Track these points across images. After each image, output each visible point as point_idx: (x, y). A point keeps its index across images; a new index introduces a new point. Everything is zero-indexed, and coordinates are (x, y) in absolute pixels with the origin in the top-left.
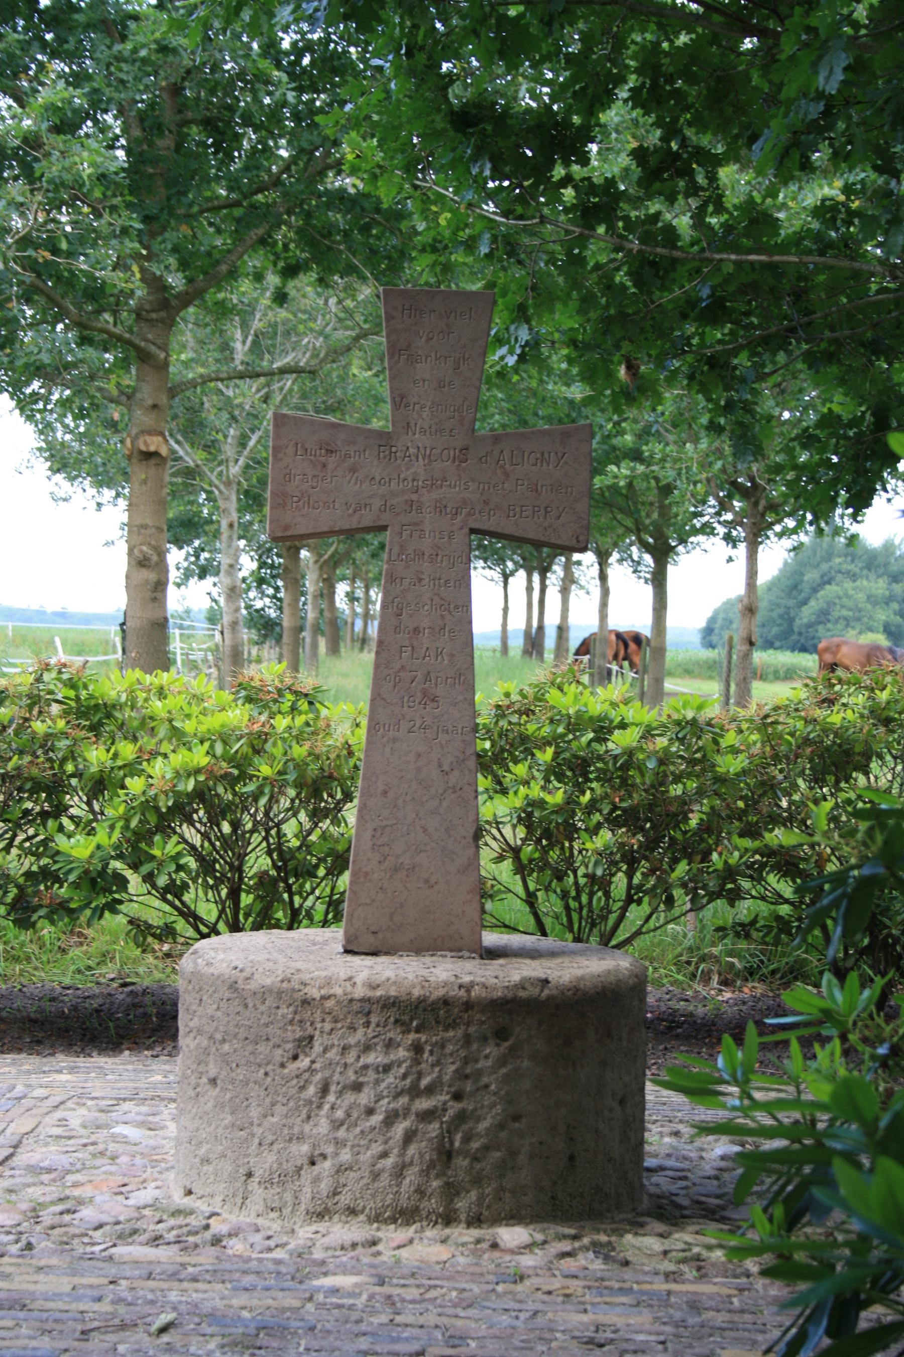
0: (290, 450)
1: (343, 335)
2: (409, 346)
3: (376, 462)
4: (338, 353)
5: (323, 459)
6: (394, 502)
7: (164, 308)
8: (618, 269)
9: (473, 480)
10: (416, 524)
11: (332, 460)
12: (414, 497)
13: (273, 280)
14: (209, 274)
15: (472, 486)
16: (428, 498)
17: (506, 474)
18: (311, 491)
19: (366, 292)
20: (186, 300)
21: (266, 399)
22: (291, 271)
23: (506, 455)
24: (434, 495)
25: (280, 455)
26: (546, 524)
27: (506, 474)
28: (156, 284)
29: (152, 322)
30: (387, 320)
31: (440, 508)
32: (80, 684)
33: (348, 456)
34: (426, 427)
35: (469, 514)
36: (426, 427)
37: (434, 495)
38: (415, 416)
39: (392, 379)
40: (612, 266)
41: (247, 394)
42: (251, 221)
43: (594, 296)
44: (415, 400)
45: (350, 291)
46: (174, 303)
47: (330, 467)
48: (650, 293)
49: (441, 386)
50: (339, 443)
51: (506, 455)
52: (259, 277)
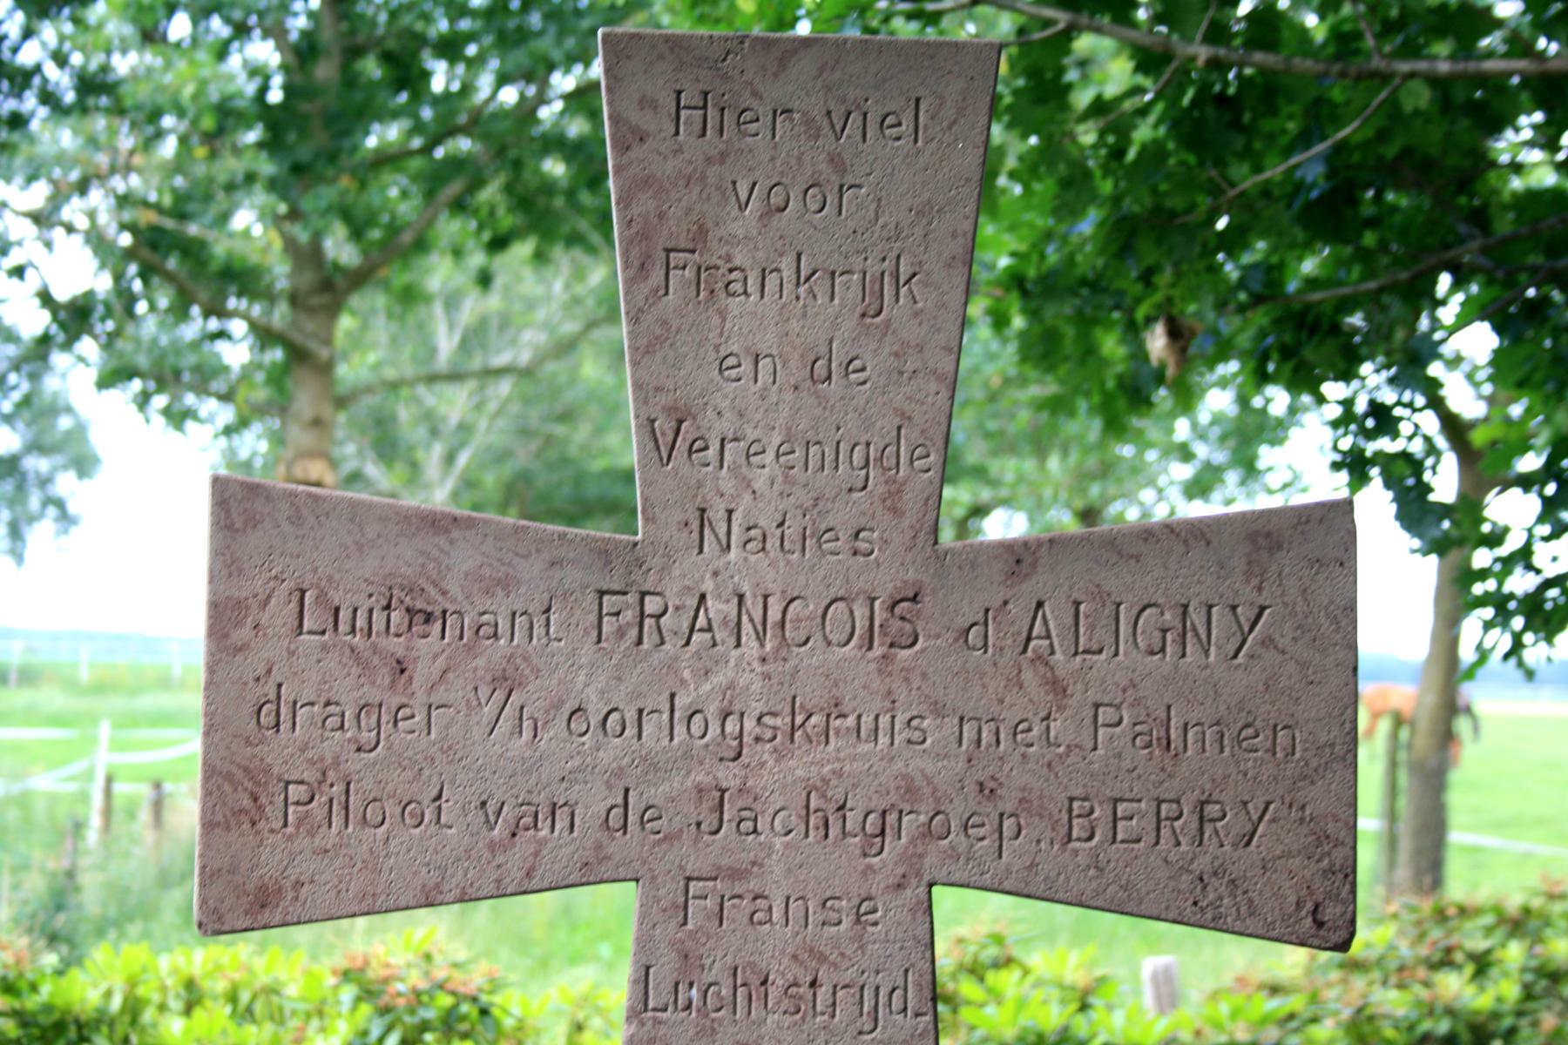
0: (279, 613)
1: (570, 328)
2: (701, 233)
3: (587, 651)
4: (565, 348)
5: (396, 645)
6: (657, 794)
7: (327, 289)
8: (1143, 111)
9: (938, 710)
10: (736, 874)
11: (428, 649)
12: (729, 776)
13: (477, 259)
14: (397, 248)
15: (937, 731)
16: (778, 777)
17: (1057, 687)
18: (355, 763)
19: (597, 275)
20: (359, 278)
21: (479, 407)
22: (499, 244)
23: (1056, 615)
24: (803, 765)
25: (243, 634)
26: (1202, 864)
27: (1057, 687)
28: (308, 256)
29: (312, 311)
30: (622, 147)
31: (822, 814)
32: (23, 985)
33: (486, 631)
34: (767, 522)
35: (927, 833)
36: (767, 522)
37: (803, 765)
38: (727, 483)
39: (643, 351)
40: (1128, 105)
41: (454, 403)
42: (450, 185)
43: (1087, 175)
44: (727, 426)
45: (579, 275)
46: (340, 282)
47: (423, 672)
48: (1220, 163)
49: (817, 373)
50: (453, 586)
51: (1056, 615)
52: (458, 253)
